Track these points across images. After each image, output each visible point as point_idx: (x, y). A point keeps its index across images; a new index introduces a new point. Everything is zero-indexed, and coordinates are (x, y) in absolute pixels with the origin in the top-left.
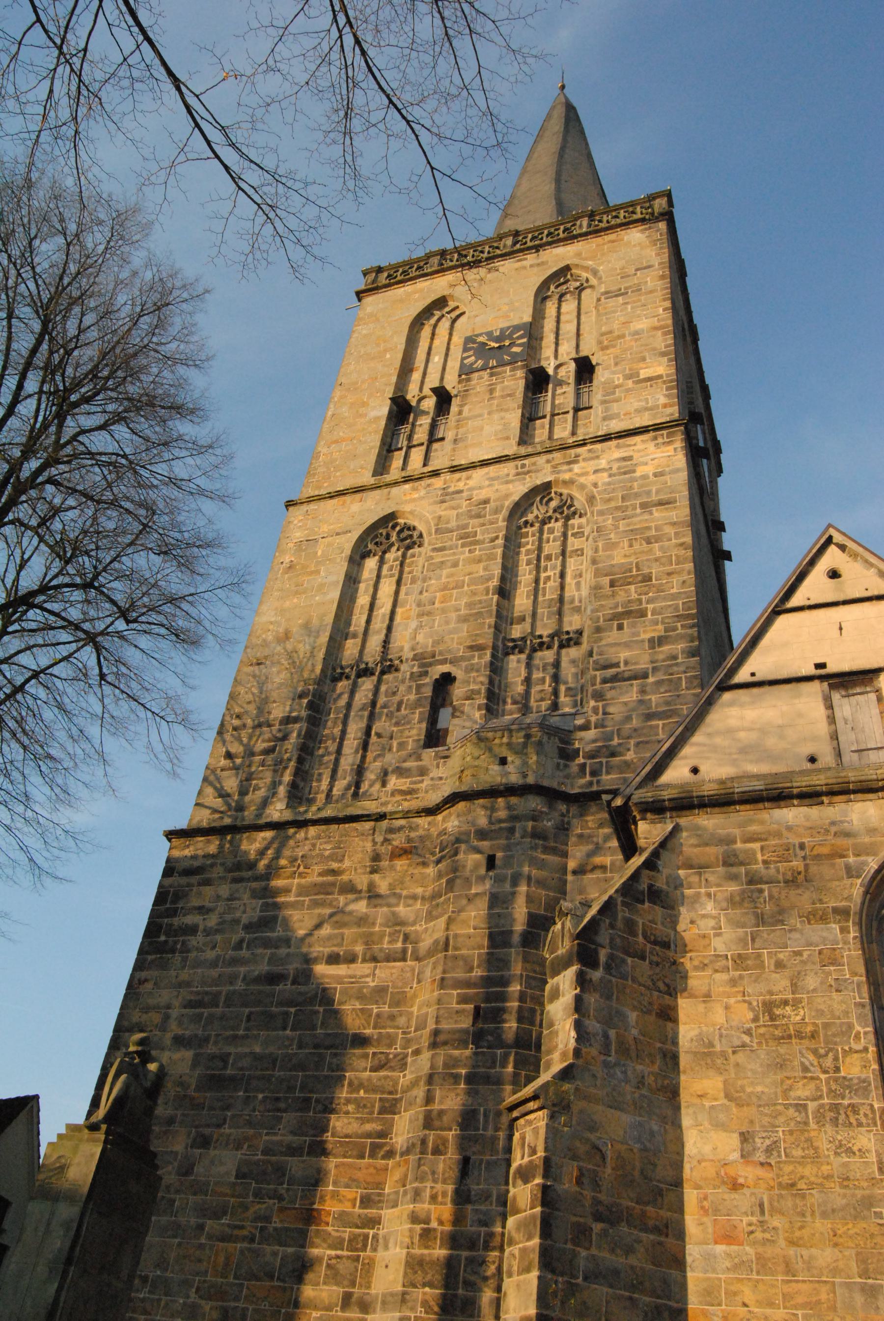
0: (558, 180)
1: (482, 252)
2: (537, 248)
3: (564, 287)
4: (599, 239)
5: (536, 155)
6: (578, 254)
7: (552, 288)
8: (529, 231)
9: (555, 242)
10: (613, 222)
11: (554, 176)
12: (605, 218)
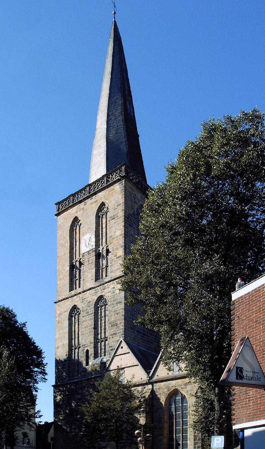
2: (95, 194)
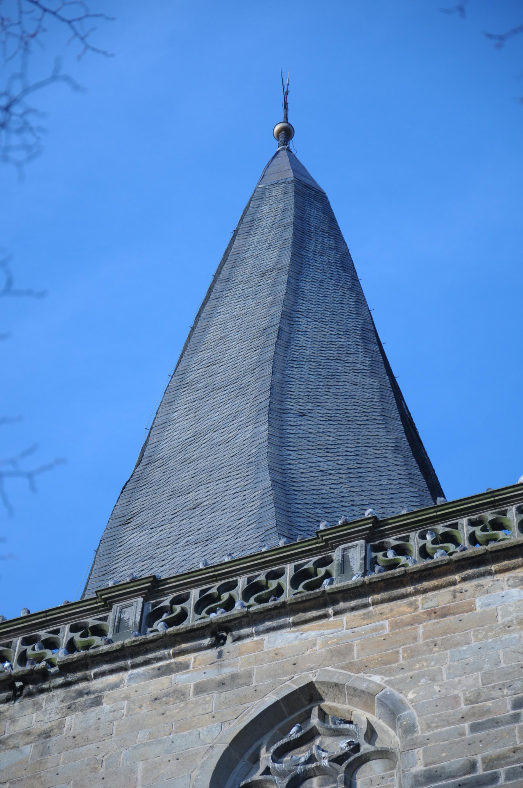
0: (277, 411)
1: (51, 644)
2: (218, 634)
3: (301, 755)
4: (401, 605)
5: (211, 336)
6: (341, 652)
7: (265, 757)
8: (192, 578)
9: (272, 613)
10: (439, 556)
11: (264, 399)
12: (415, 542)
